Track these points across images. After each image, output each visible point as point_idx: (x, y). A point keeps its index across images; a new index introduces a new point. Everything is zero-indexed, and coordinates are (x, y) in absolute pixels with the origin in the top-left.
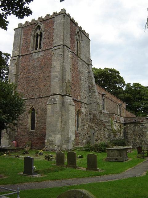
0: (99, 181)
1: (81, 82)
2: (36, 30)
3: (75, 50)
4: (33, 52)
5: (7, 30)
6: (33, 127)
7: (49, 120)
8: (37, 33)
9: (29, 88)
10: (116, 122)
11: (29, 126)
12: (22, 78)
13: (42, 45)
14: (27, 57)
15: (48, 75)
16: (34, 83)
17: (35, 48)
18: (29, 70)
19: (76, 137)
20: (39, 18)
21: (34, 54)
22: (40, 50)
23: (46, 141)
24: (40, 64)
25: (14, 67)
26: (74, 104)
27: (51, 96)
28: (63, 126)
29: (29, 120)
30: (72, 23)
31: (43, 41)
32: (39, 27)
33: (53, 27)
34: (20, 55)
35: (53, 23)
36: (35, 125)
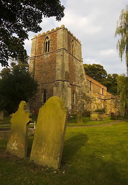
3: (71, 52)
13: (50, 49)
15: (54, 68)
16: (45, 74)
17: (45, 51)
21: (44, 55)
24: (49, 61)
26: (70, 86)
27: (56, 82)
31: (50, 46)
34: (36, 56)
35: (56, 34)
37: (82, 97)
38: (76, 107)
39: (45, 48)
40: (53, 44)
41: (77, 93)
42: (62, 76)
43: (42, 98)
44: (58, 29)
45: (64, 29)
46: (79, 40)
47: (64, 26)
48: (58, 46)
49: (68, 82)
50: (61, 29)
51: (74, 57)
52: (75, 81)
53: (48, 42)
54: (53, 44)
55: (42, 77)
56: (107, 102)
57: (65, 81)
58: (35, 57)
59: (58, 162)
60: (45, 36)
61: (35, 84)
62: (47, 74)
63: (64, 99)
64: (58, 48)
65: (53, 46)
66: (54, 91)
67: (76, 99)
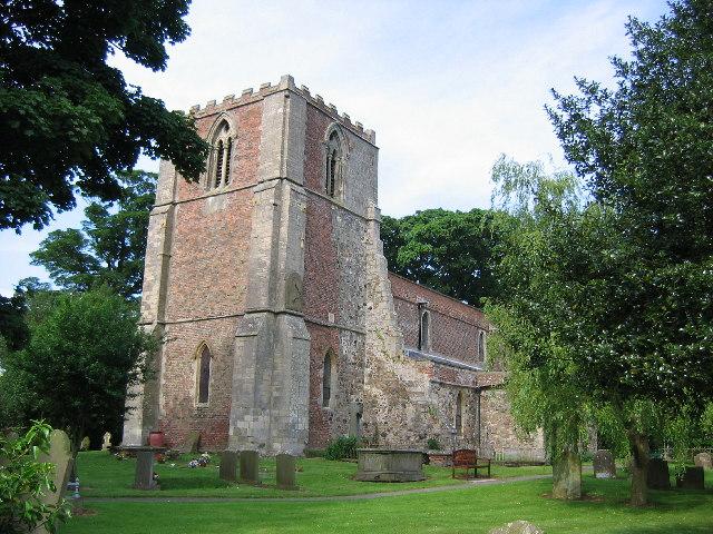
0: (427, 525)
1: (342, 274)
2: (217, 133)
3: (319, 187)
4: (208, 194)
5: (163, 69)
6: (203, 395)
7: (240, 377)
8: (221, 142)
9: (196, 291)
10: (441, 384)
11: (194, 392)
12: (179, 265)
13: (232, 176)
14: (195, 205)
15: (242, 257)
16: (208, 279)
17: (213, 182)
18: (196, 243)
19: (311, 423)
20: (227, 99)
21: (210, 199)
22: (227, 189)
23: (231, 432)
24: (225, 227)
25: (158, 233)
26: (307, 335)
27: (246, 316)
28: (275, 394)
29: (195, 377)
30: (313, 110)
31: (234, 164)
32: (225, 125)
33: (260, 128)
34: (177, 200)
35: (259, 114)
36: (210, 389)
37: (370, 375)
38: (338, 419)
39: (224, 159)
40: (247, 157)
41: (345, 359)
42: (272, 290)
43: (194, 379)
44: (268, 91)
45: (287, 93)
46: (366, 128)
47: (291, 79)
48: (261, 167)
49: (296, 319)
50: (278, 95)
51: (335, 205)
52: (336, 311)
53: (225, 142)
54: (247, 157)
55: (196, 291)
56: (486, 398)
57: (284, 313)
58: (174, 204)
59: (135, 404)
60: (214, 119)
61: (608, 105)
62: (215, 281)
63: (277, 390)
64: (262, 173)
65: (243, 161)
66: (238, 352)
67: (340, 386)
